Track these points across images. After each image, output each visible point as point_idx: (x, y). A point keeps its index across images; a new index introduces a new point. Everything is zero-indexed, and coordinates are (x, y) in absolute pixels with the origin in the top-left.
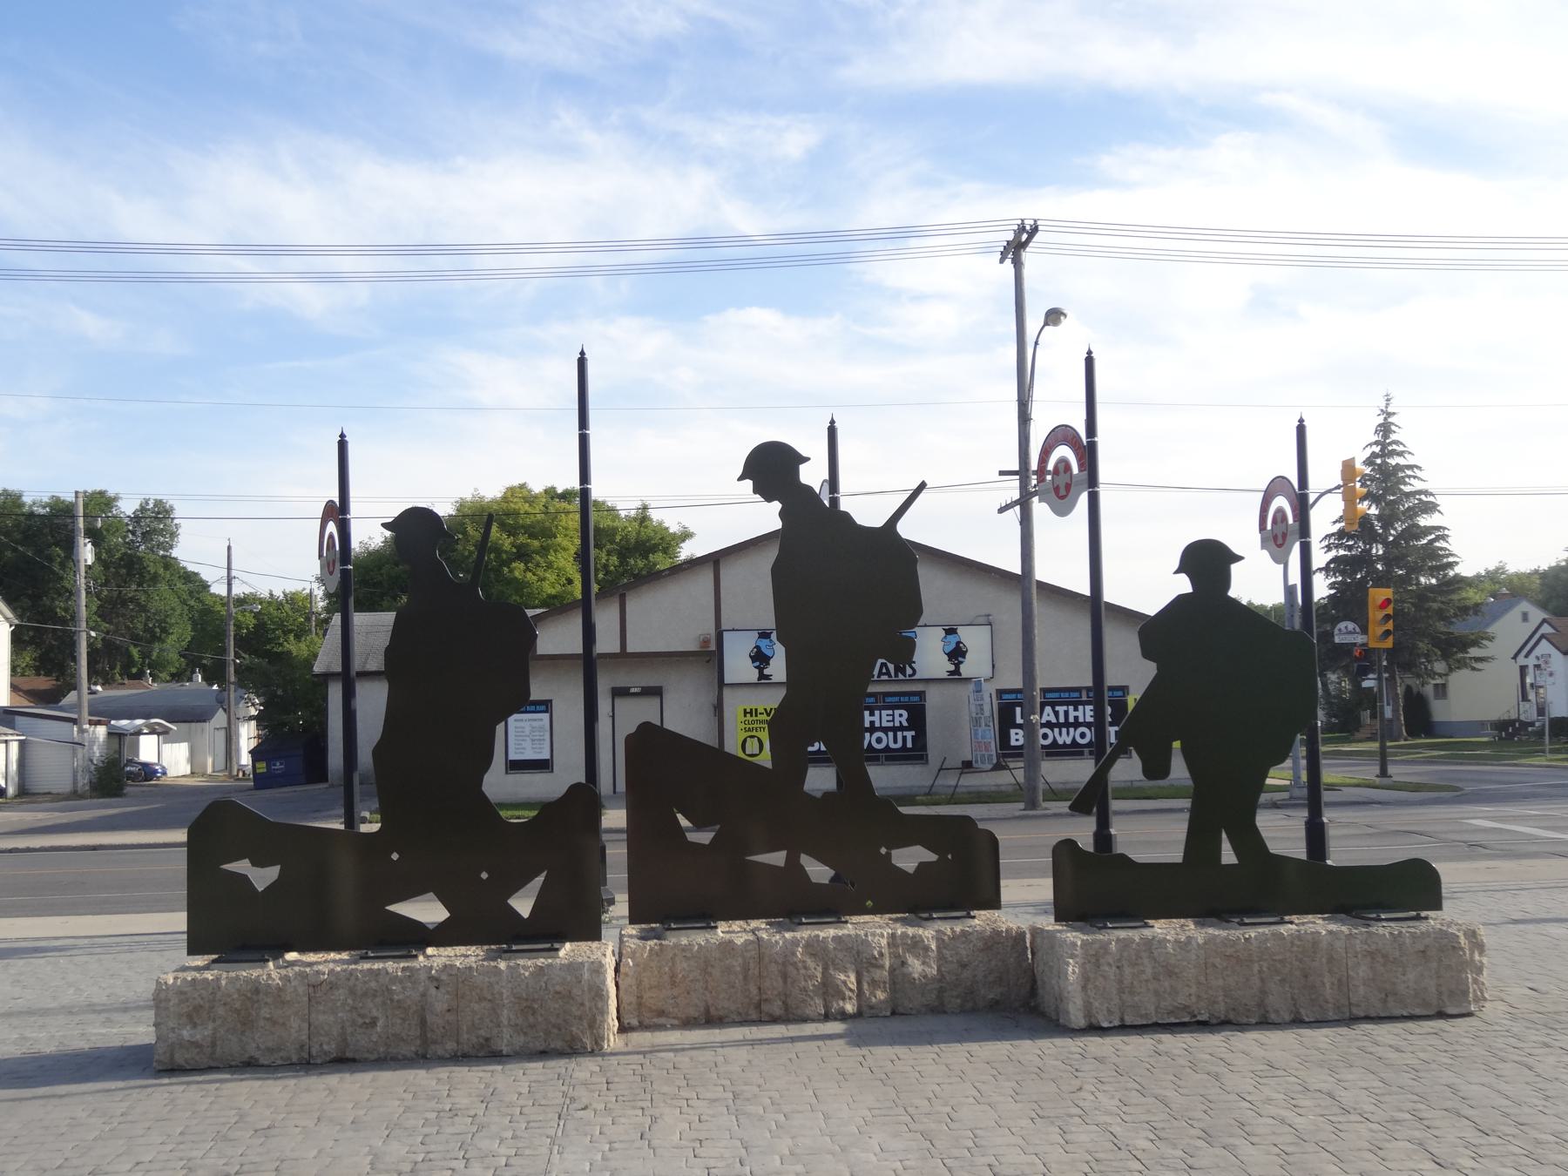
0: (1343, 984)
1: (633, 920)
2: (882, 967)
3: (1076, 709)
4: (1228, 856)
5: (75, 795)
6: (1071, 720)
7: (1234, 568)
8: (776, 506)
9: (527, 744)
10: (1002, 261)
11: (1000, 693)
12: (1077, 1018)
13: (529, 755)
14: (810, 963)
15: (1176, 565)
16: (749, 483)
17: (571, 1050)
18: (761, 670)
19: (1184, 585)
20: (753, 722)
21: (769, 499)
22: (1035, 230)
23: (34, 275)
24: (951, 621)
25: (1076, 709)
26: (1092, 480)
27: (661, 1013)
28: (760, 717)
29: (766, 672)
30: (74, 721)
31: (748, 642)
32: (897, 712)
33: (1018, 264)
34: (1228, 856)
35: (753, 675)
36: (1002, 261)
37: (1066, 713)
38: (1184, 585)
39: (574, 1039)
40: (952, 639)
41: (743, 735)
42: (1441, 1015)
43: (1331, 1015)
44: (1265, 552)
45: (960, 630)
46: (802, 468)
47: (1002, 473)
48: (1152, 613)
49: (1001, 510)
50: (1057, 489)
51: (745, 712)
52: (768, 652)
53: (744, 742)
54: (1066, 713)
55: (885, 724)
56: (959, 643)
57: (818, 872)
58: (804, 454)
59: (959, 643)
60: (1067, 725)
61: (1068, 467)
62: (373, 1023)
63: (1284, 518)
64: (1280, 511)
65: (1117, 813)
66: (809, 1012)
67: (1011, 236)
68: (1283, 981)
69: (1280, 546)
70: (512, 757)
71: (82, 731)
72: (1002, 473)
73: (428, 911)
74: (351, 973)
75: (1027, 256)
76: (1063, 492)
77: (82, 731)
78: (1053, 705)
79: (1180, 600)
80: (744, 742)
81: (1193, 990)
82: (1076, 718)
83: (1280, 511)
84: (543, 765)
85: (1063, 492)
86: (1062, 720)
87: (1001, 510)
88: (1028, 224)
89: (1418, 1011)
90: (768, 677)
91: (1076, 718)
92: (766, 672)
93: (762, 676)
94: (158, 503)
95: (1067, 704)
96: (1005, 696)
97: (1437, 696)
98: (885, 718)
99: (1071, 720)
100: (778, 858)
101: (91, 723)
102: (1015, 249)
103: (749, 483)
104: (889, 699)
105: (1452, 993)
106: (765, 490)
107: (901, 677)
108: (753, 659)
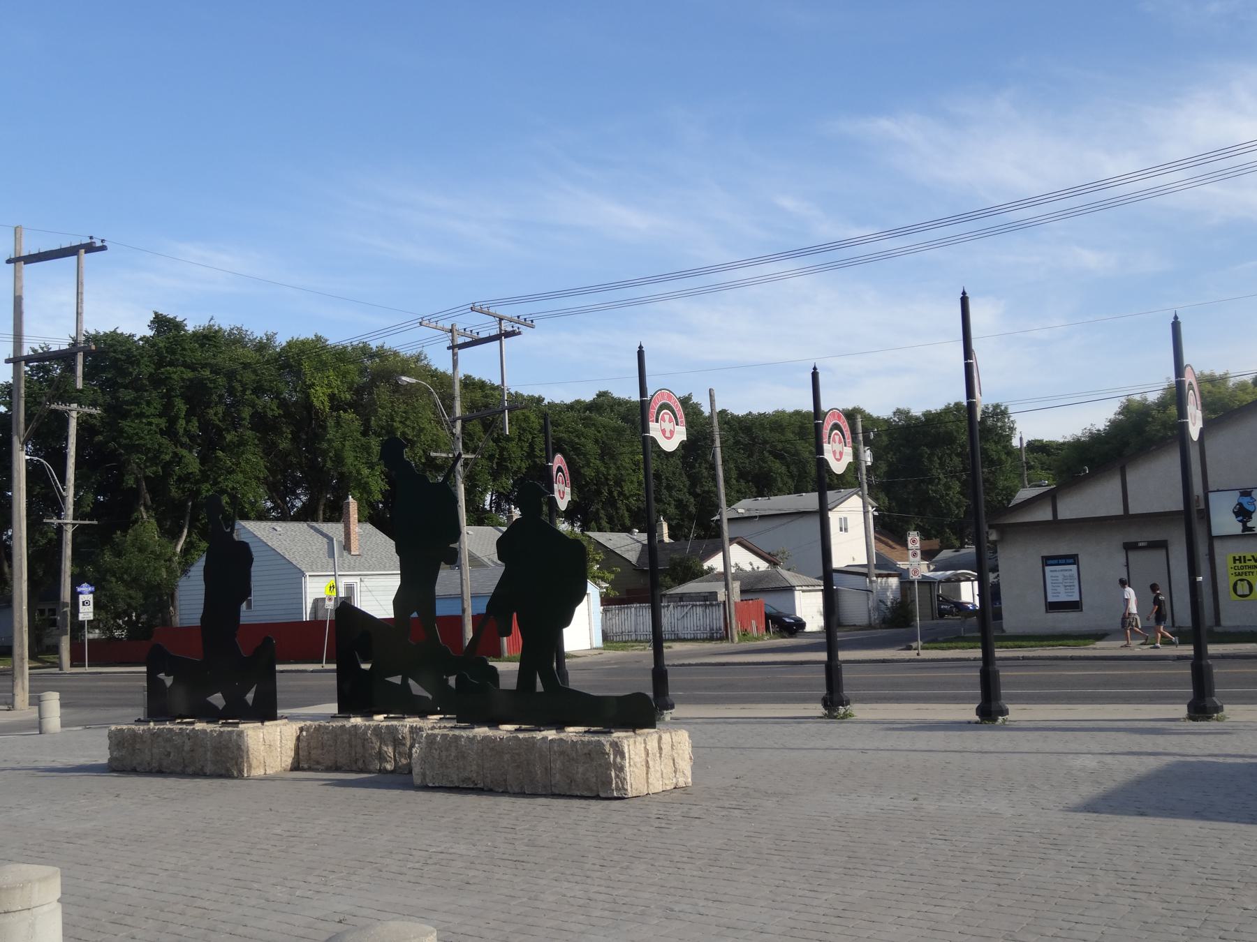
0: (548, 771)
2: (404, 745)
4: (540, 687)
5: (870, 626)
9: (1061, 589)
12: (417, 780)
13: (1063, 598)
14: (374, 739)
17: (228, 776)
18: (1244, 523)
20: (1242, 568)
23: (888, 255)
24: (1247, 485)
27: (318, 763)
28: (1249, 563)
29: (1249, 524)
30: (866, 575)
31: (1232, 499)
34: (540, 687)
35: (1237, 528)
39: (228, 770)
41: (1234, 579)
42: (597, 797)
43: (540, 791)
48: (391, 544)
51: (1235, 560)
52: (1250, 508)
53: (1235, 585)
57: (416, 688)
62: (169, 754)
65: (1214, 657)
66: (371, 768)
68: (518, 767)
70: (1050, 600)
71: (871, 582)
73: (217, 699)
74: (457, 738)
76: (668, 434)
77: (871, 582)
80: (1235, 585)
81: (474, 767)
84: (1075, 606)
85: (668, 434)
89: (585, 793)
90: (1251, 529)
92: (1249, 524)
93: (1245, 528)
94: (997, 406)
100: (397, 680)
101: (878, 576)
105: (603, 783)
108: (1237, 514)
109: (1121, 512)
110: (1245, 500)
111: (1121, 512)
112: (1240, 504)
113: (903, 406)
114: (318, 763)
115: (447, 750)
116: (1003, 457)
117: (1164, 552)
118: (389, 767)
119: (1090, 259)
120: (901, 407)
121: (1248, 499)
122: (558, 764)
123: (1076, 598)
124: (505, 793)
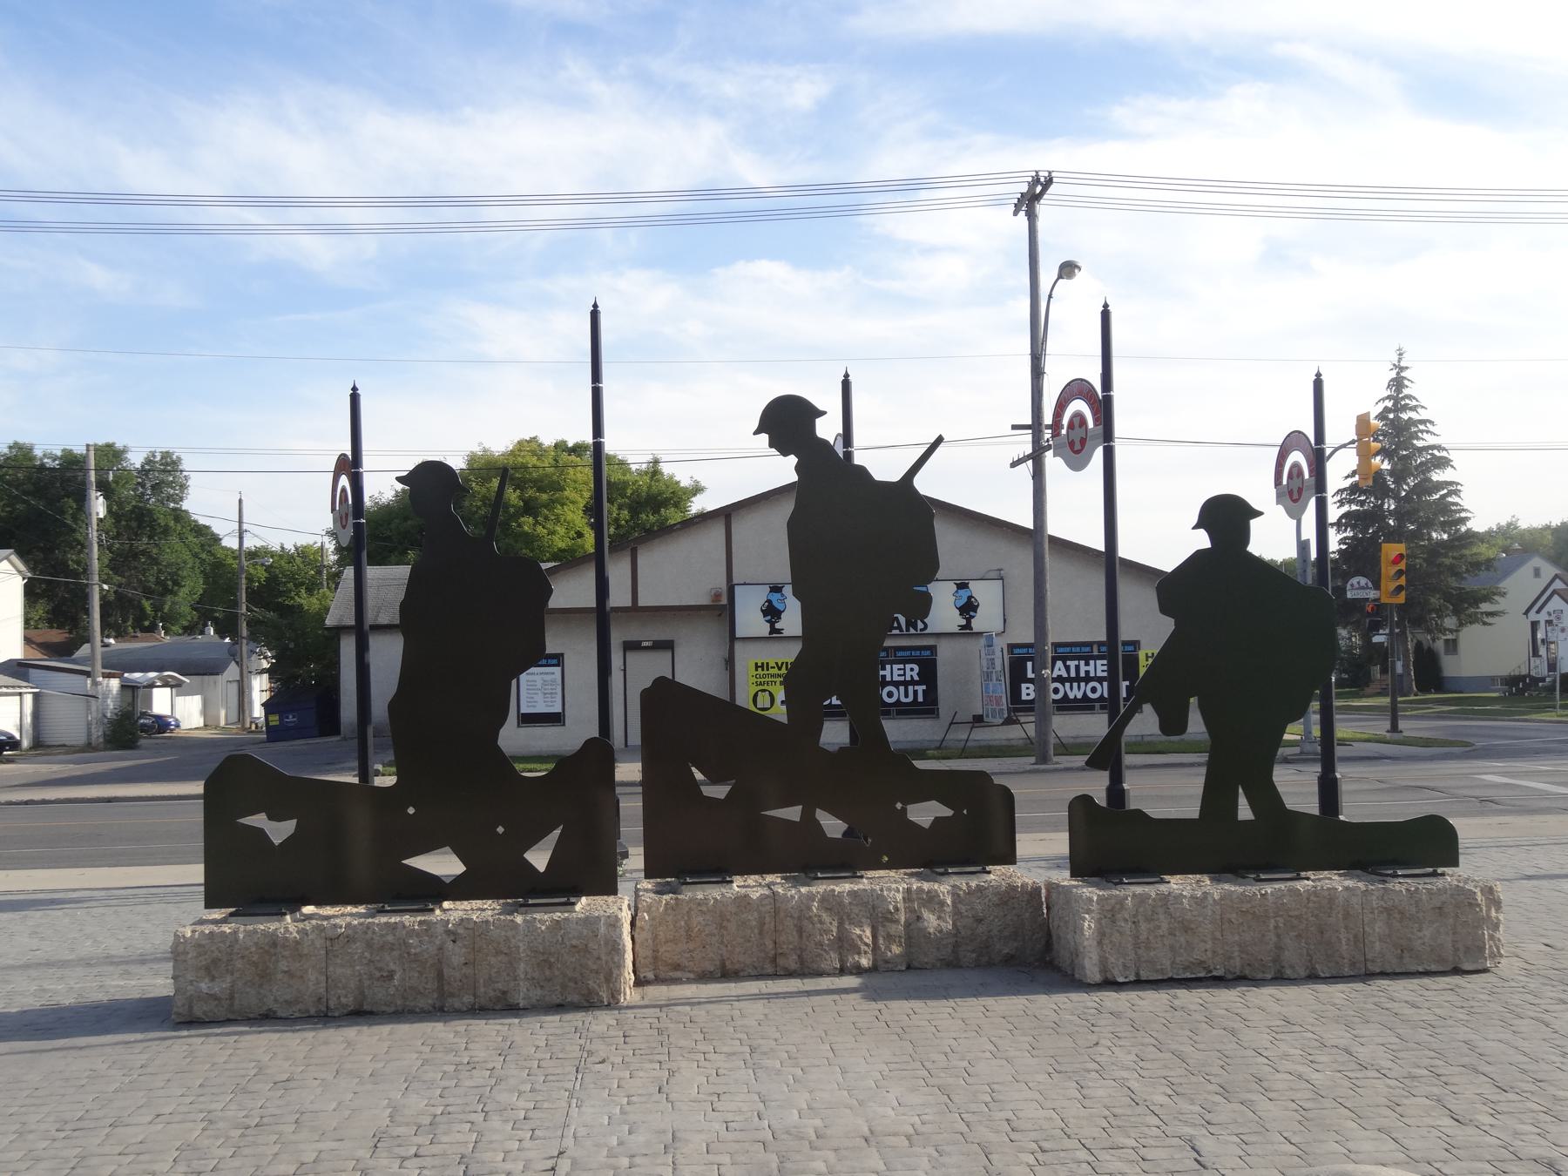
0: (1359, 940)
1: (649, 874)
2: (897, 922)
3: (1087, 664)
4: (1245, 812)
5: (89, 747)
6: (1082, 674)
7: (1254, 523)
8: (792, 460)
9: (539, 697)
10: (1015, 213)
11: (1012, 647)
12: (1093, 973)
13: (541, 708)
14: (825, 917)
15: (1195, 520)
16: (765, 437)
17: (589, 1003)
18: (772, 624)
19: (1202, 540)
20: (764, 676)
21: (785, 453)
22: (1049, 181)
25: (1087, 664)
26: (1108, 435)
27: (677, 967)
28: (772, 671)
29: (777, 626)
30: (88, 674)
31: (759, 596)
32: (908, 666)
33: (1032, 217)
34: (1245, 812)
35: (763, 629)
36: (1015, 213)
37: (1077, 667)
38: (1202, 540)
39: (590, 992)
40: (964, 594)
42: (1457, 971)
43: (1347, 971)
44: (1281, 508)
45: (972, 584)
46: (819, 421)
47: (1014, 427)
49: (1014, 465)
50: (1071, 444)
51: (757, 667)
53: (756, 696)
54: (1077, 667)
55: (896, 678)
56: (970, 597)
57: (833, 826)
58: (821, 408)
59: (970, 597)
60: (1078, 679)
61: (1083, 422)
62: (391, 976)
63: (1300, 473)
64: (1296, 466)
67: (1025, 188)
69: (1295, 501)
72: (1014, 427)
73: (444, 864)
75: (1042, 209)
76: (1078, 447)
77: (95, 684)
78: (1064, 659)
79: (1199, 556)
80: (756, 696)
82: (1087, 672)
83: (1296, 466)
84: (555, 719)
85: (1078, 447)
86: (1073, 674)
87: (1014, 465)
88: (1043, 175)
89: (1433, 968)
90: (779, 631)
91: (1087, 672)
92: (777, 626)
93: (773, 630)
95: (1079, 658)
96: (1017, 651)
97: (1447, 652)
98: (896, 672)
99: (1082, 674)
100: (793, 813)
101: (106, 676)
102: (1029, 202)
103: (765, 437)
104: (900, 654)
106: (782, 444)
107: (912, 631)
108: (765, 613)
109: (629, 604)
110: (775, 597)
111: (629, 604)
112: (769, 601)
113: (23, 439)
114: (677, 967)
115: (1149, 920)
116: (172, 523)
117: (669, 654)
118: (865, 962)
119: (98, 277)
120: (21, 440)
121: (778, 596)
122: (1379, 927)
123: (557, 709)
124: (1280, 979)
